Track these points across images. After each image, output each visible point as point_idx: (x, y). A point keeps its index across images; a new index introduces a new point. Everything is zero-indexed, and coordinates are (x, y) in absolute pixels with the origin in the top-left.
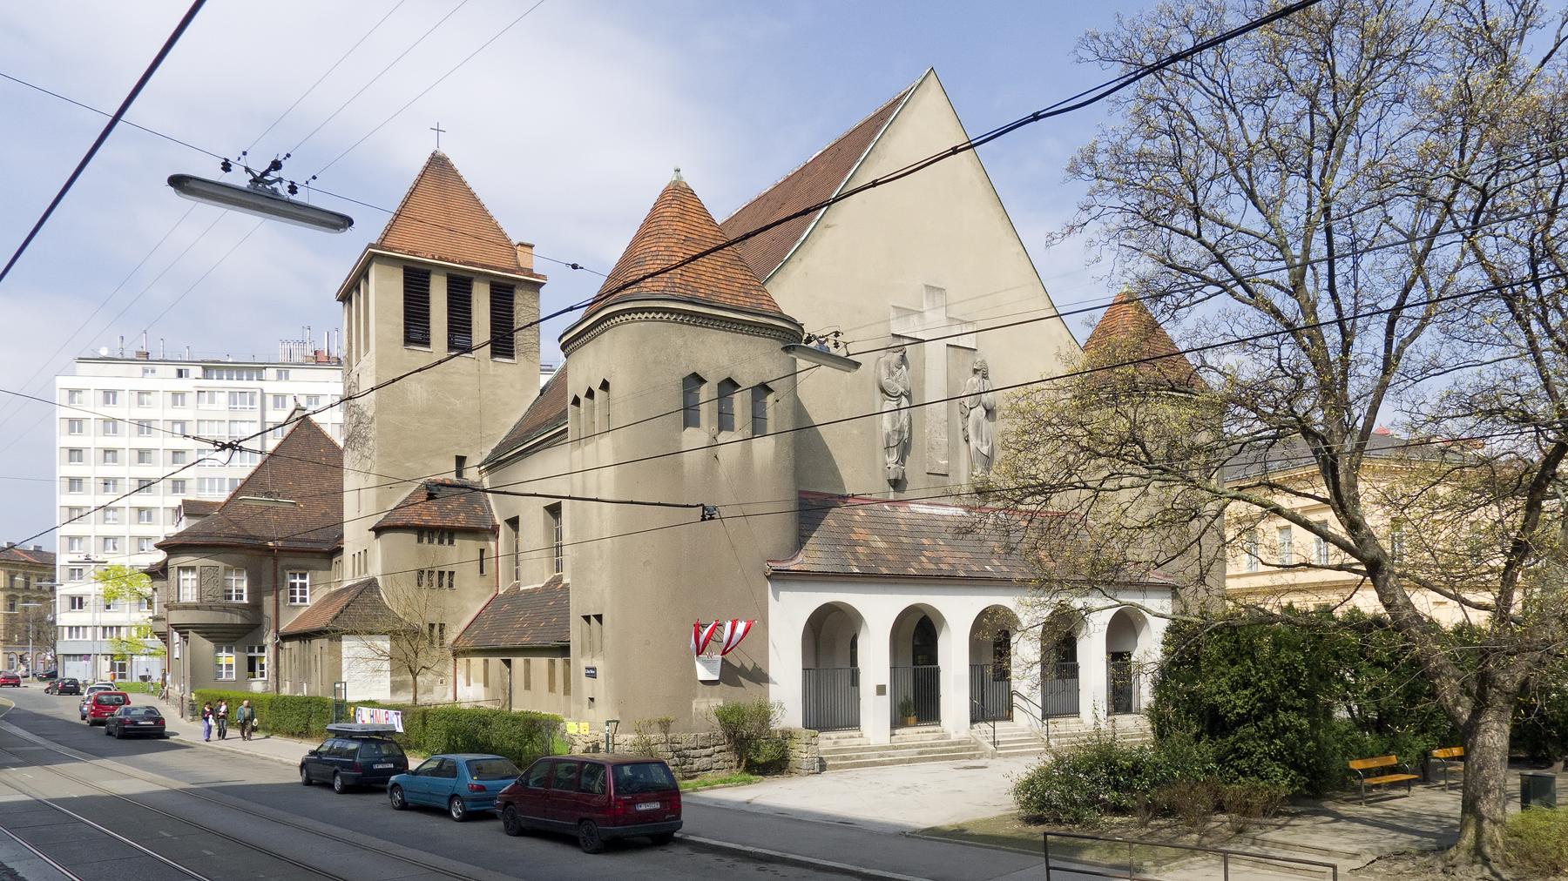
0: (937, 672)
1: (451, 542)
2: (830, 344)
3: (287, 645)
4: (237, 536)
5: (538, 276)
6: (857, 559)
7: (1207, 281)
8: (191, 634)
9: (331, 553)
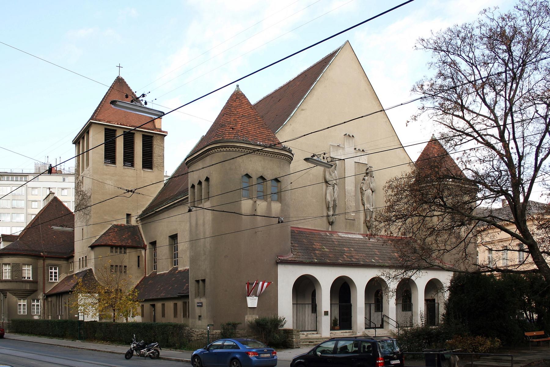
0: (351, 305)
1: (125, 253)
2: (322, 158)
3: (49, 299)
4: (27, 250)
5: (164, 132)
6: (316, 256)
7: (467, 134)
8: (8, 294)
9: (69, 257)
